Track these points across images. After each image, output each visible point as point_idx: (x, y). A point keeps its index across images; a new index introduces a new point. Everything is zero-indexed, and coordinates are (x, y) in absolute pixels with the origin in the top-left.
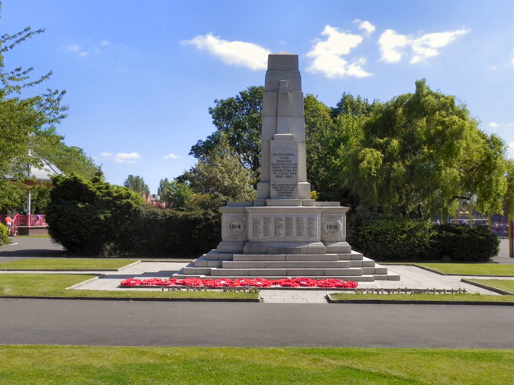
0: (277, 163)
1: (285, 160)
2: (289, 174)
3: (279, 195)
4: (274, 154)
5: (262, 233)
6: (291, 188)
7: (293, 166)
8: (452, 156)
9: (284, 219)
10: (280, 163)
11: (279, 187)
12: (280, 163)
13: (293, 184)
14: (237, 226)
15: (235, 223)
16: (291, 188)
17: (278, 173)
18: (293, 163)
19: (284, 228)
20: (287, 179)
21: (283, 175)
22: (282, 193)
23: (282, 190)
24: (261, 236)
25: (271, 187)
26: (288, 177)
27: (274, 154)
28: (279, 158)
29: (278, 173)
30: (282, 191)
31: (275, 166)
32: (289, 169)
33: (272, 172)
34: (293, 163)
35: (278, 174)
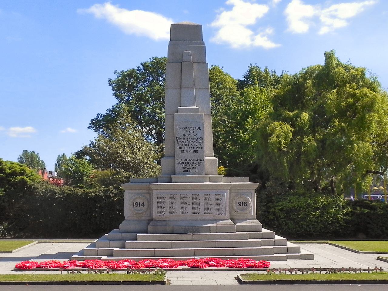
0: (182, 137)
2: (195, 149)
5: (168, 211)
7: (199, 140)
8: (364, 129)
9: (191, 196)
10: (186, 137)
12: (186, 137)
14: (141, 204)
15: (138, 201)
16: (197, 164)
17: (183, 147)
19: (191, 206)
21: (189, 150)
22: (188, 168)
23: (188, 165)
24: (167, 214)
25: (176, 162)
26: (194, 151)
28: (184, 132)
29: (183, 147)
30: (188, 166)
31: (180, 140)
32: (195, 143)
33: (176, 146)
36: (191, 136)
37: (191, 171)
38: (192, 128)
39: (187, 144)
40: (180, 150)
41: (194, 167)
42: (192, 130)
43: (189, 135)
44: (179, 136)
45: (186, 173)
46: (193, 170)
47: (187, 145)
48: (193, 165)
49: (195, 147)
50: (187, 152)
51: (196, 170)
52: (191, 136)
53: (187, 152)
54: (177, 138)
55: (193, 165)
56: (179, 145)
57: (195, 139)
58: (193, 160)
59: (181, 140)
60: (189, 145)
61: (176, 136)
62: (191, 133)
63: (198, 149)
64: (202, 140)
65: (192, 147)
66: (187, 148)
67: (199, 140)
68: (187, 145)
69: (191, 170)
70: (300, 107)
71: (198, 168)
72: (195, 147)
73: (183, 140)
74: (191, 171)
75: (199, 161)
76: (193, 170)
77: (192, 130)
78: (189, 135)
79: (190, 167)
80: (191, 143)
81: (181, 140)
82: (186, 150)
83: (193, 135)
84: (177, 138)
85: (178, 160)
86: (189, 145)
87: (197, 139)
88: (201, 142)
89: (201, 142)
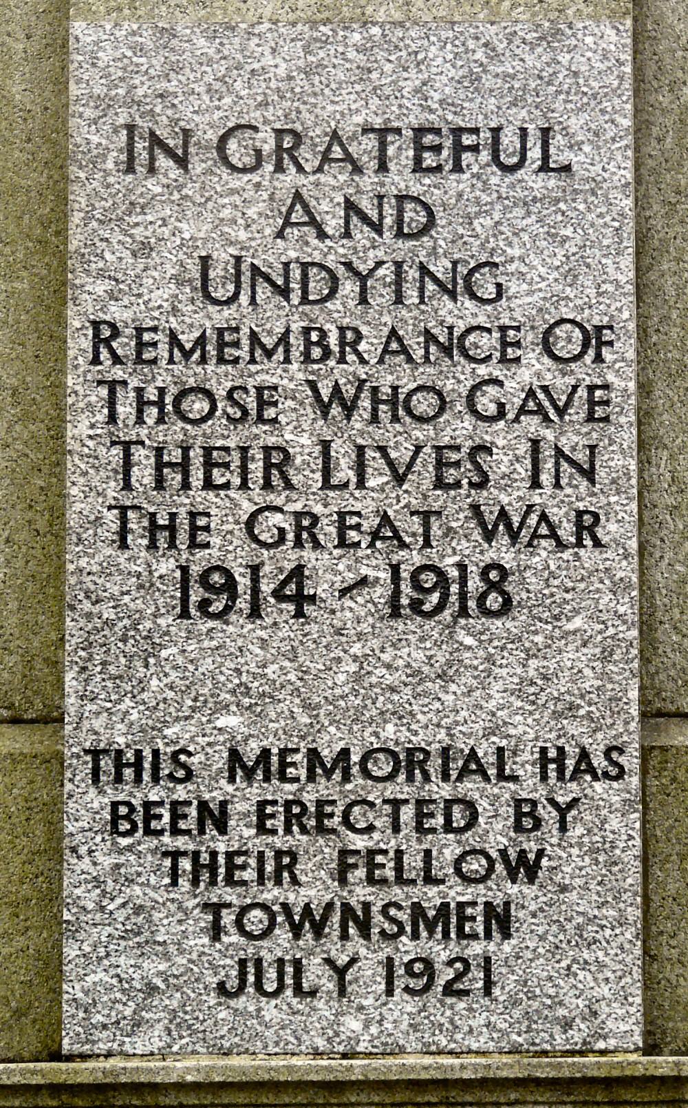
0: (197, 320)
1: (370, 249)
2: (461, 551)
3: (249, 975)
4: (156, 148)
6: (496, 833)
7: (533, 368)
8: (606, 1089)
10: (276, 316)
11: (244, 798)
12: (276, 316)
13: (528, 731)
16: (496, 833)
17: (226, 511)
18: (522, 303)
20: (417, 644)
21: (327, 569)
22: (310, 922)
25: (86, 805)
26: (422, 596)
27: (156, 148)
28: (234, 216)
29: (226, 511)
30: (314, 888)
32: (459, 428)
33: (89, 495)
34: (522, 303)
35: (227, 548)
36: (381, 296)
37: (369, 970)
38: (401, 153)
39: (303, 445)
40: (166, 566)
41: (432, 897)
42: (401, 178)
43: (349, 288)
44: (157, 297)
45: (270, 1010)
46: (408, 948)
47: (307, 475)
48: (413, 862)
49: (455, 507)
50: (301, 600)
51: (476, 948)
52: (381, 296)
53: (301, 600)
54: (103, 335)
55: (413, 862)
56: (143, 474)
57: (454, 346)
58: (411, 762)
59: (191, 374)
60: (345, 472)
61: (90, 297)
62: (389, 247)
63: (503, 552)
64: (584, 372)
65: (399, 504)
66: (306, 529)
67: (533, 368)
68: (307, 475)
69: (369, 961)
70: (265, 964)
71: (500, 920)
72: (455, 507)
73: (220, 379)
74: (369, 970)
75: (531, 786)
76: (408, 948)
77: (401, 178)
78: (349, 288)
79: (360, 893)
80: (387, 432)
81: (191, 374)
82: (289, 557)
83: (413, 274)
84: (103, 335)
85: (110, 764)
86: (345, 472)
87: (487, 343)
88: (577, 413)
89: (577, 413)
